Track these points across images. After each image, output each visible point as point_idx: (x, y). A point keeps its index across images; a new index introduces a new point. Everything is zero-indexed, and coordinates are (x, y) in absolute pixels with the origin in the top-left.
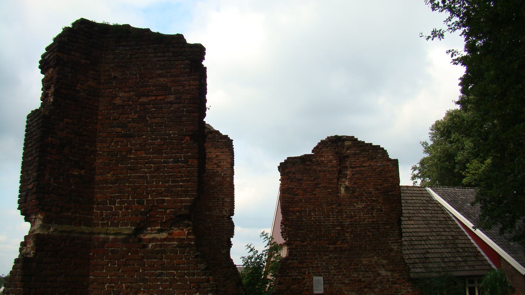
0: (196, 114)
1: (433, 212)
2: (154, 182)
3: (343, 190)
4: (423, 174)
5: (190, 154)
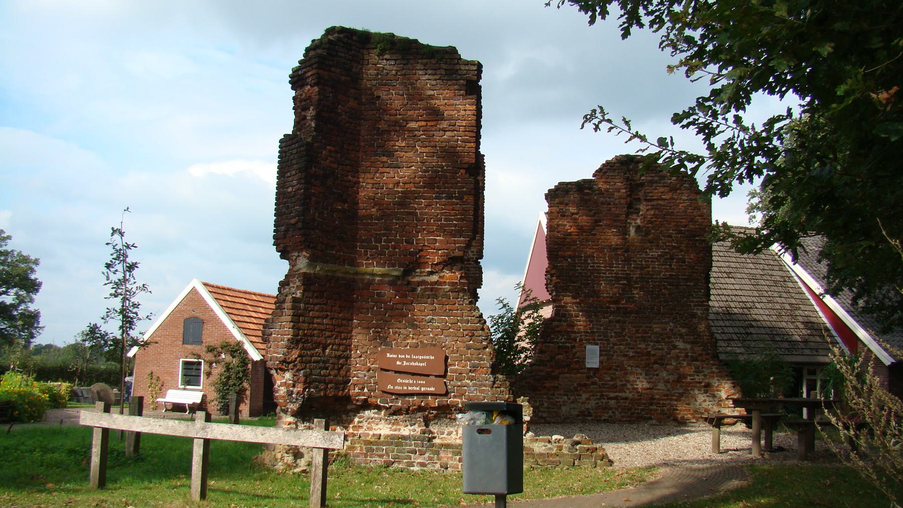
0: (472, 144)
1: (766, 267)
3: (632, 231)
5: (465, 189)
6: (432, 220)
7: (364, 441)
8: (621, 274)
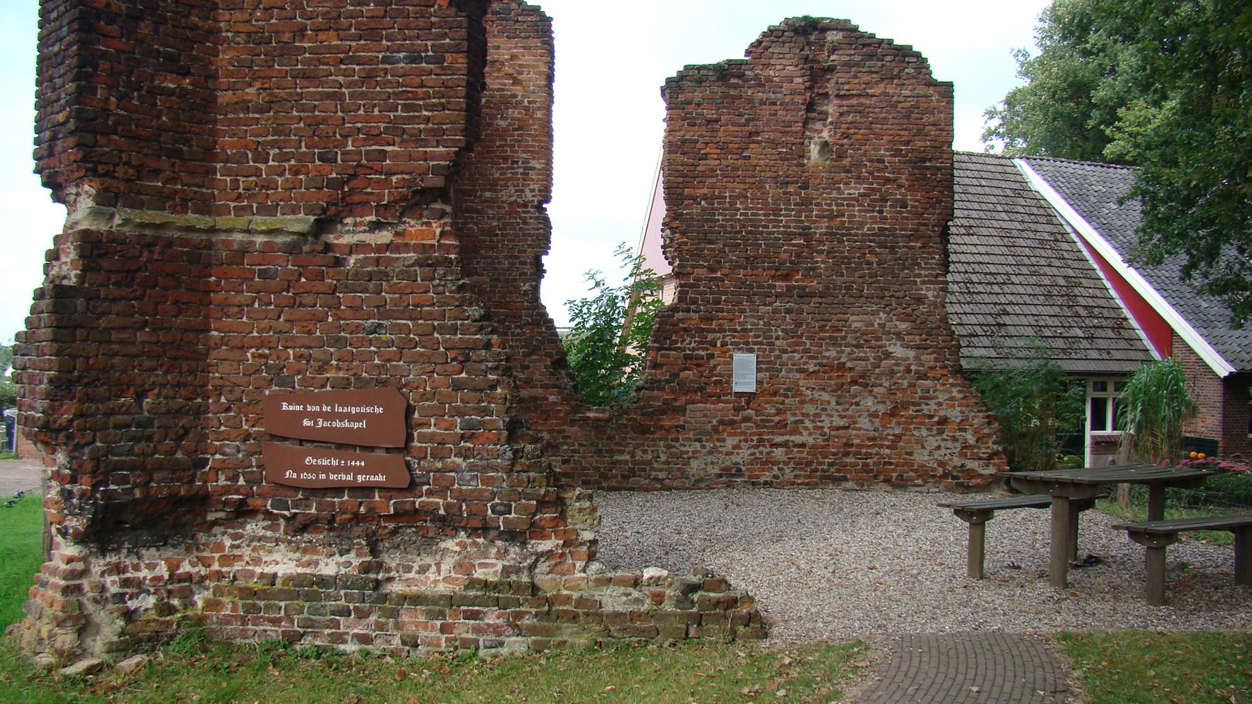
1: (1027, 218)
2: (359, 109)
3: (814, 150)
4: (1010, 131)
5: (447, 41)
6: (376, 110)
7: (241, 590)
8: (794, 227)
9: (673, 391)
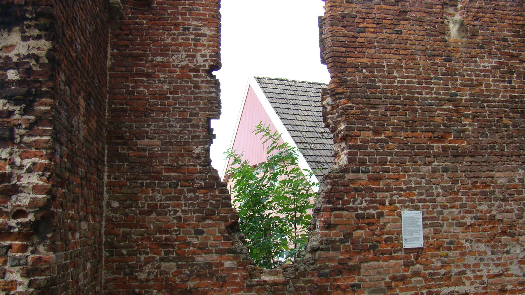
8: (444, 94)
9: (347, 251)
